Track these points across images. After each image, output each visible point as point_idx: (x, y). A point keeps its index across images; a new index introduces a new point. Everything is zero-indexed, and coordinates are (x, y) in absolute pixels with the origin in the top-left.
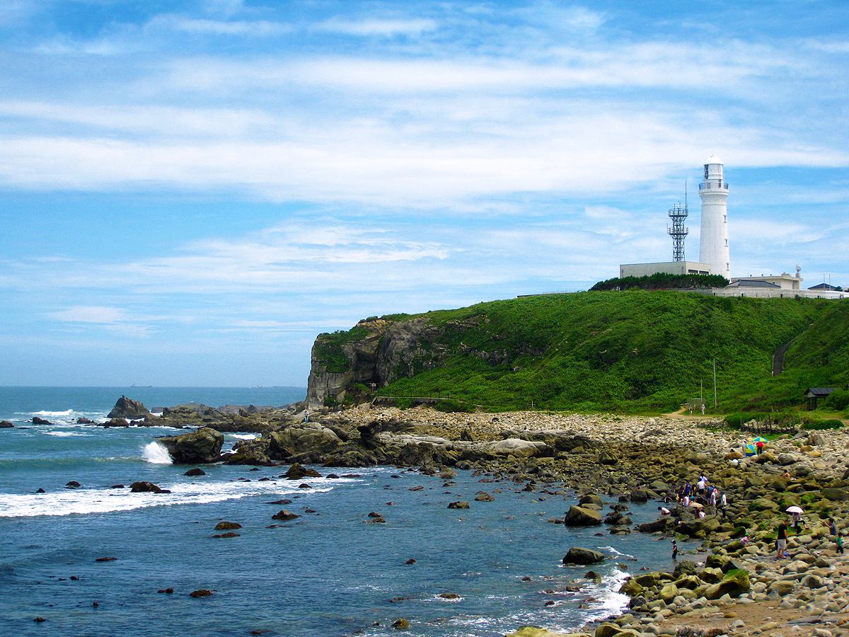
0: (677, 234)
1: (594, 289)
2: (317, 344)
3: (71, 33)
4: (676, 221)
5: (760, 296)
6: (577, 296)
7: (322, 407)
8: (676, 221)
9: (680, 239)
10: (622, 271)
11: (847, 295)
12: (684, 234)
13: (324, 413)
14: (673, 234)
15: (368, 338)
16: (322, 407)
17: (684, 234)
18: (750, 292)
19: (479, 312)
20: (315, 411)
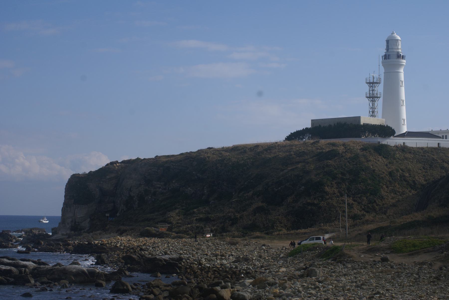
0: (372, 98)
1: (289, 138)
2: (70, 181)
3: (362, 123)
4: (372, 86)
5: (419, 146)
6: (270, 148)
7: (68, 232)
8: (372, 86)
9: (375, 101)
10: (312, 124)
11: (446, 144)
12: (377, 97)
13: (69, 236)
14: (370, 97)
15: (108, 177)
16: (68, 232)
17: (377, 97)
18: (411, 143)
19: (188, 158)
20: (63, 235)
